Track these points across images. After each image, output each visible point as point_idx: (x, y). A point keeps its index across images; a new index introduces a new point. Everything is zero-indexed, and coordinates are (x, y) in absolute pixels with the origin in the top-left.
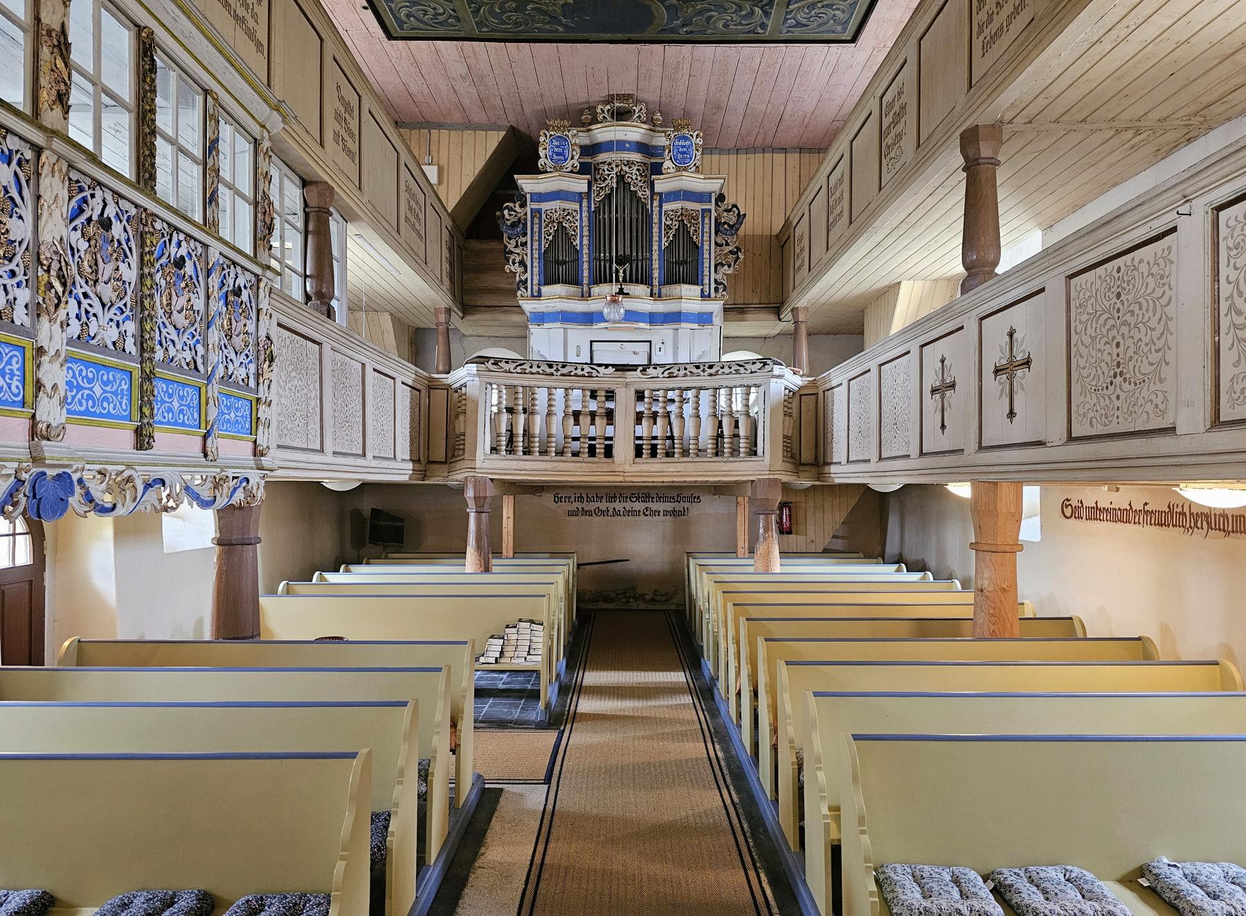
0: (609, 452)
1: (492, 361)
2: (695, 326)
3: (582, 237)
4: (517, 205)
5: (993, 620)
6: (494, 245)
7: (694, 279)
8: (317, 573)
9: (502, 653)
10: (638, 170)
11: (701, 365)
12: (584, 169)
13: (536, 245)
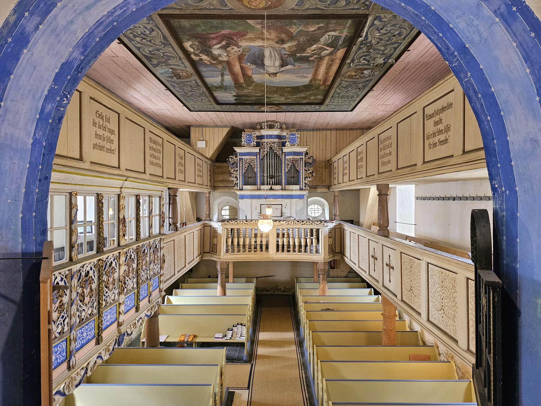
0: (267, 248)
1: (226, 221)
2: (298, 199)
3: (257, 168)
4: (234, 157)
5: (388, 339)
6: (225, 164)
7: (297, 183)
9: (232, 335)
10: (277, 145)
11: (299, 221)
12: (258, 145)
13: (241, 171)
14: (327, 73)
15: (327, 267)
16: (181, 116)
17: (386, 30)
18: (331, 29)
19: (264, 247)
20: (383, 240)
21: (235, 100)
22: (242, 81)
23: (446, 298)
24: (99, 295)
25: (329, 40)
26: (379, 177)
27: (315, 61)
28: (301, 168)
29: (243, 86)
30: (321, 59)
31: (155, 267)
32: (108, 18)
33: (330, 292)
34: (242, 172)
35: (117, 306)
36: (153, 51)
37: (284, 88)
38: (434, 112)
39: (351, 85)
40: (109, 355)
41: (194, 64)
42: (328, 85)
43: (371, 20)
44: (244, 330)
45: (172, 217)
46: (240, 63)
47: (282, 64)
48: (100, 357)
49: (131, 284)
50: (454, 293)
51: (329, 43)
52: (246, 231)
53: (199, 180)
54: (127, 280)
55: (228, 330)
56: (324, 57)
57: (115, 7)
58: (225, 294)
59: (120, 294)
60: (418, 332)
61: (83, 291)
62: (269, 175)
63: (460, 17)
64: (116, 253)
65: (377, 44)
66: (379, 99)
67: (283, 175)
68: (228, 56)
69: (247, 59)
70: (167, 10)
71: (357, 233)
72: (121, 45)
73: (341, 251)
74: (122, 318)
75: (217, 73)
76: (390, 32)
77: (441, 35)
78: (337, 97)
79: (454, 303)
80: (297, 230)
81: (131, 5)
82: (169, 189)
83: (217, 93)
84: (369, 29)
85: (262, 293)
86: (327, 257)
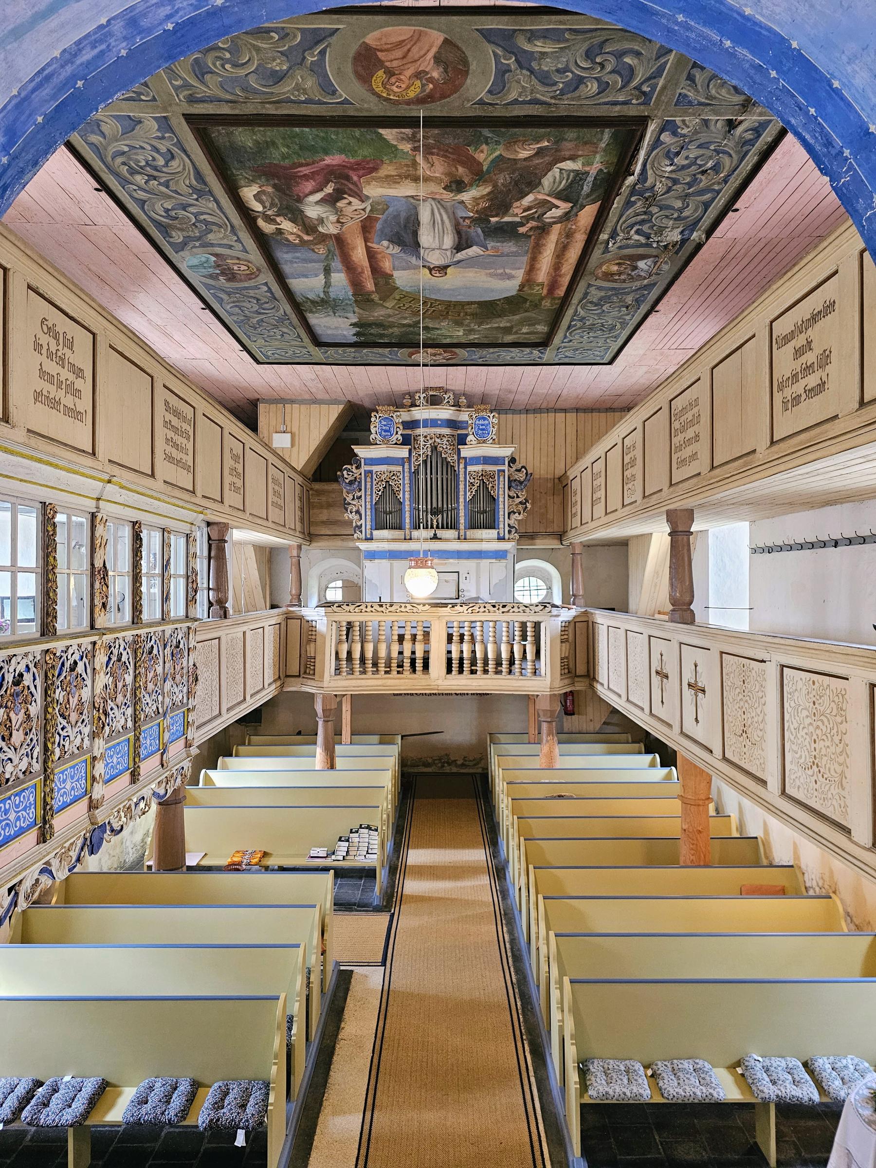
0: (426, 666)
1: (336, 605)
2: (494, 561)
4: (354, 467)
5: (692, 852)
6: (334, 486)
7: (492, 525)
8: (203, 771)
9: (348, 852)
12: (406, 441)
13: (368, 498)
14: (557, 266)
15: (558, 708)
16: (238, 376)
17: (687, 158)
18: (567, 154)
19: (419, 664)
20: (680, 632)
21: (354, 335)
22: (370, 285)
23: (824, 737)
24: (46, 732)
25: (560, 183)
26: (672, 493)
27: (530, 236)
28: (501, 492)
29: (373, 300)
30: (543, 230)
31: (176, 690)
32: (62, 66)
33: (562, 762)
34: (371, 501)
35: (88, 762)
36: (173, 209)
37: (462, 305)
38: (793, 328)
39: (609, 297)
40: (69, 871)
41: (263, 242)
42: (559, 298)
43: (653, 131)
44: (375, 839)
45: (215, 587)
46: (366, 240)
47: (459, 242)
48: (46, 870)
49: (120, 718)
50: (841, 723)
51: (562, 190)
52: (381, 628)
53: (275, 514)
54: (112, 709)
55: (340, 840)
56: (551, 224)
57: (79, 42)
58: (332, 767)
59: (94, 735)
60: (759, 840)
61: (8, 716)
62: (429, 507)
63: (857, 58)
64: (86, 642)
65: (667, 192)
66: (671, 334)
67: (462, 507)
68: (338, 221)
69: (382, 231)
70: (201, 105)
71: (624, 626)
72: (103, 194)
73: (588, 671)
74: (98, 791)
75: (316, 265)
76: (694, 163)
77: (812, 111)
78: (579, 328)
79: (841, 746)
80: (491, 624)
81: (116, 40)
82: (209, 524)
83: (317, 318)
84: (648, 155)
85: (415, 770)
86: (558, 683)
